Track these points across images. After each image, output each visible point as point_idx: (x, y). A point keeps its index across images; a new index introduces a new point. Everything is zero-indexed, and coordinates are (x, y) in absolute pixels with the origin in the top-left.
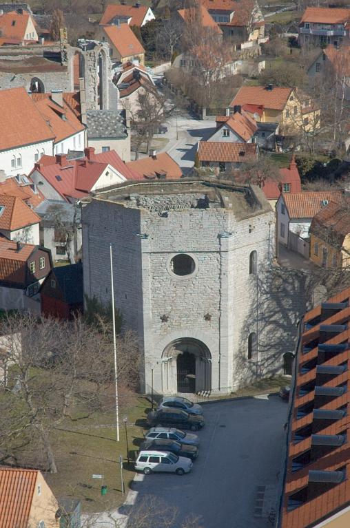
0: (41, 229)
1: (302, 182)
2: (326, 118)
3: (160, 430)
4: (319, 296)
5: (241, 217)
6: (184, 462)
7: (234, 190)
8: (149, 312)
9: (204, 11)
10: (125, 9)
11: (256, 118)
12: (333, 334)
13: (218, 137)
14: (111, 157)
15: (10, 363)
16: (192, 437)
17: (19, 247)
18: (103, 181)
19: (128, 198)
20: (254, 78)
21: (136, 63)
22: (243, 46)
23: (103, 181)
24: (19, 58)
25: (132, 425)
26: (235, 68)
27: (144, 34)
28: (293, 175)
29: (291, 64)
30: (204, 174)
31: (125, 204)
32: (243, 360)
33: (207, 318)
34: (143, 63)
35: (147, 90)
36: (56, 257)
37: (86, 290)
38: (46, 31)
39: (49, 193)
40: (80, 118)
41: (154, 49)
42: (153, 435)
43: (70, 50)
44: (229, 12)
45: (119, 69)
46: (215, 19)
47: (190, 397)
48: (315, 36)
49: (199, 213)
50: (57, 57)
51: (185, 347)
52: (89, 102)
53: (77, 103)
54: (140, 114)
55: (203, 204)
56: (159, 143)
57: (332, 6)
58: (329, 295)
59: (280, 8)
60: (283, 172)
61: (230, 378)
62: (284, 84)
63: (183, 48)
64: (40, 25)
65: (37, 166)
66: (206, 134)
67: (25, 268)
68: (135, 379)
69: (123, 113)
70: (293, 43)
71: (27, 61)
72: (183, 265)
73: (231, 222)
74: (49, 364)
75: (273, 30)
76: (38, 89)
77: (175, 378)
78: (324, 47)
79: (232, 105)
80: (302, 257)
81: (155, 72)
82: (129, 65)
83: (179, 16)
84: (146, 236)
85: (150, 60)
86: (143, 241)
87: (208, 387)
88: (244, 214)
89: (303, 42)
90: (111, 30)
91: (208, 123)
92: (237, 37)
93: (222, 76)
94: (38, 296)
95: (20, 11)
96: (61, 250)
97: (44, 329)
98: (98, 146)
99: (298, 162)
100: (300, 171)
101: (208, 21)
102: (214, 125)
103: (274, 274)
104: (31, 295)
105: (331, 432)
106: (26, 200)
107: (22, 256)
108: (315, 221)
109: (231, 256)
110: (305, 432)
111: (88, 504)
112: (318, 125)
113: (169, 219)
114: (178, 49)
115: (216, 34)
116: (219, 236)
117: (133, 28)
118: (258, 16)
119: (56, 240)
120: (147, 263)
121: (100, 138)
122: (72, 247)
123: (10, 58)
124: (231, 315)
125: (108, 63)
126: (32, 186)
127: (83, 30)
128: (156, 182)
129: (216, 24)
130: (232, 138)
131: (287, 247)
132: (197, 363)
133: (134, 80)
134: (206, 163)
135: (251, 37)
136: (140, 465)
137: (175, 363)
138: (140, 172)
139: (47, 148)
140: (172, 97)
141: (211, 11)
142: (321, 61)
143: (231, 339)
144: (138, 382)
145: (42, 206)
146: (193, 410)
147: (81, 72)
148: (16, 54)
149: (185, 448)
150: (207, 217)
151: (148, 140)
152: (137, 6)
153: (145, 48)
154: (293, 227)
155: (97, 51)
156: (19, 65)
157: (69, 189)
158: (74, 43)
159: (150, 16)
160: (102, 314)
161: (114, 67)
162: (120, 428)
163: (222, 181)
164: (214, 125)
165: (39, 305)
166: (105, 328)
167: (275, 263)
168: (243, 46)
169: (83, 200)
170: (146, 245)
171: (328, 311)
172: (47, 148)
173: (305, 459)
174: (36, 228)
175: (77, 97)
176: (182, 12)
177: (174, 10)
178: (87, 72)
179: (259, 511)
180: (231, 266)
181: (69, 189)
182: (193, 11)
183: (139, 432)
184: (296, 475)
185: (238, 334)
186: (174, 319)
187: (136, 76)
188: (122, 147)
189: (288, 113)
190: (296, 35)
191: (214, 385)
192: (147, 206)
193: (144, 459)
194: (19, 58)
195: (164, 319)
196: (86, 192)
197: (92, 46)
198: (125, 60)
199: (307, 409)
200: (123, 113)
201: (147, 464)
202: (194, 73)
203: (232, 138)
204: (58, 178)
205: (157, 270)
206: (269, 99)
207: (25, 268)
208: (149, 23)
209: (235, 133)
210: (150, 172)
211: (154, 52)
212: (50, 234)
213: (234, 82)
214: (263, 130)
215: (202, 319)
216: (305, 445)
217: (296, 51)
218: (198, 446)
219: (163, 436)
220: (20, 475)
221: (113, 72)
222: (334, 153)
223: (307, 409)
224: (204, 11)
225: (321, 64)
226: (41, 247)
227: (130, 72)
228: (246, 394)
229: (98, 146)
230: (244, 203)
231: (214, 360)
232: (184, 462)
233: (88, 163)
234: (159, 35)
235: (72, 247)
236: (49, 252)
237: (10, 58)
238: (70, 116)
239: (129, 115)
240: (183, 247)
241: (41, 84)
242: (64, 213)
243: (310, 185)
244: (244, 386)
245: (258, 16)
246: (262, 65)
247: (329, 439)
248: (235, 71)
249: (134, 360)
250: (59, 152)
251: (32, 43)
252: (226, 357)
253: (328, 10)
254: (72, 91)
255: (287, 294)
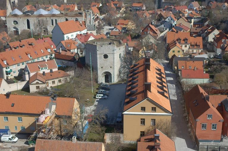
0: (77, 49)
1: (132, 39)
2: (137, 26)
3: (101, 90)
4: (134, 62)
5: (117, 46)
6: (106, 96)
7: (116, 41)
8: (99, 66)
9: (112, 4)
10: (96, 4)
11: (122, 26)
12: (136, 70)
13: (114, 30)
14: (92, 34)
15: (70, 77)
16: (108, 92)
17: (72, 53)
18: (90, 39)
19: (94, 43)
20: (122, 18)
21: (98, 15)
22: (120, 11)
23: (90, 39)
24: (73, 14)
25: (96, 89)
26: (118, 16)
27: (99, 9)
28: (129, 38)
29: (130, 15)
30: (111, 38)
31: (94, 44)
32: (119, 75)
33: (111, 67)
34: (99, 15)
35: (100, 20)
36: (80, 55)
37: (86, 62)
38: (79, 8)
39: (79, 42)
40: (85, 26)
41: (102, 12)
42: (100, 91)
43: (84, 12)
44: (117, 4)
45: (94, 16)
46: (114, 5)
47: (108, 84)
48: (135, 9)
49: (109, 46)
50: (81, 14)
51: (106, 73)
52: (88, 23)
53: (85, 23)
54: (98, 25)
55: (110, 44)
56: (102, 31)
57: (138, 3)
58: (136, 62)
59: (128, 3)
60: (127, 37)
61: (116, 80)
62: (128, 19)
63: (107, 11)
64: (78, 7)
65: (76, 36)
66: (112, 29)
67: (74, 57)
68: (96, 80)
69: (95, 25)
70: (131, 10)
71: (75, 15)
72: (106, 56)
73: (116, 48)
74: (78, 77)
75: (126, 8)
76: (77, 20)
77: (104, 80)
78: (137, 11)
79: (117, 23)
80: (131, 55)
81: (101, 17)
82: (96, 15)
83: (107, 5)
84: (98, 51)
85: (101, 14)
86: (97, 52)
87: (111, 81)
88: (118, 46)
89: (133, 10)
90: (93, 8)
91: (112, 27)
92: (119, 9)
93: (115, 18)
94: (76, 63)
95: (74, 4)
96: (81, 54)
97: (77, 70)
98: (89, 32)
99: (131, 35)
100: (131, 37)
101: (113, 6)
102: (114, 28)
103: (125, 59)
104: (75, 63)
105: (134, 90)
106: (74, 43)
107: (73, 55)
108: (134, 47)
109: (115, 55)
110: (129, 90)
111: (86, 105)
112: (135, 28)
113: (103, 47)
114: (107, 12)
115: (114, 9)
116: (113, 50)
117: (97, 7)
118: (123, 5)
119: (80, 52)
120: (98, 56)
121: (90, 30)
122: (84, 53)
123: (71, 14)
124: (116, 67)
125: (92, 15)
126: (75, 41)
127: (87, 8)
128: (102, 39)
129: (114, 7)
130: (117, 30)
131: (128, 53)
132: (109, 77)
133: (174, 44)
134: (112, 36)
135: (122, 9)
136: (97, 97)
137: (104, 77)
138: (98, 37)
139: (79, 33)
140: (105, 22)
141: (113, 4)
142: (136, 14)
143: (116, 72)
144: (97, 80)
145: (77, 45)
146: (108, 86)
147: (86, 17)
148: (72, 13)
149: (106, 94)
150: (111, 47)
151: (100, 31)
152: (98, 3)
153: (100, 12)
154: (129, 49)
155: (89, 12)
156: (73, 15)
157: (83, 41)
158: (84, 11)
159: (101, 5)
160: (89, 67)
161: (93, 16)
162: (93, 90)
163: (115, 39)
164: (114, 28)
165: (77, 65)
166: (90, 70)
167: (125, 56)
168: (120, 11)
169: (85, 43)
170: (98, 52)
171: (135, 66)
172: (79, 33)
173: (129, 95)
174: (76, 49)
175: (85, 22)
176: (107, 4)
177: (106, 4)
178: (87, 17)
179: (120, 106)
180: (116, 57)
181: (83, 41)
182: (110, 4)
183: (97, 91)
184: (127, 98)
185: (117, 71)
186: (104, 68)
187: (98, 17)
188: (94, 32)
189: (129, 25)
190: (131, 9)
191: (112, 81)
192: (98, 44)
193: (97, 96)
194: (73, 14)
195: (102, 68)
196: (86, 41)
197: (88, 11)
198: (95, 14)
199: (130, 85)
200: (95, 25)
201: (98, 97)
202: (110, 17)
203: (117, 30)
204: (81, 39)
205: (100, 58)
206: (125, 22)
207: (74, 57)
208: (101, 7)
209: (118, 29)
210: (100, 37)
211: (101, 13)
212: (79, 50)
213: (118, 19)
214: (124, 28)
215: (110, 68)
216: (129, 92)
217: (131, 12)
218: (109, 94)
219: (102, 91)
220: (71, 99)
221: (93, 17)
222: (138, 33)
223: (130, 85)
224: (112, 4)
225: (136, 15)
226: (77, 53)
227: (96, 17)
228: (121, 83)
229: (89, 32)
230: (119, 43)
231: (112, 76)
232: (106, 96)
233: (87, 36)
234: (103, 9)
235: (84, 53)
236: (79, 54)
237: (71, 14)
238: (83, 25)
239: (96, 25)
240: (105, 53)
241: (78, 19)
242: (82, 46)
243: (133, 40)
244: (119, 81)
245: (123, 5)
246: (124, 15)
247: (134, 91)
248: (118, 16)
249: (96, 76)
250: (81, 33)
251: (76, 11)
252: (115, 75)
253: (137, 4)
254: (84, 21)
255: (128, 62)
